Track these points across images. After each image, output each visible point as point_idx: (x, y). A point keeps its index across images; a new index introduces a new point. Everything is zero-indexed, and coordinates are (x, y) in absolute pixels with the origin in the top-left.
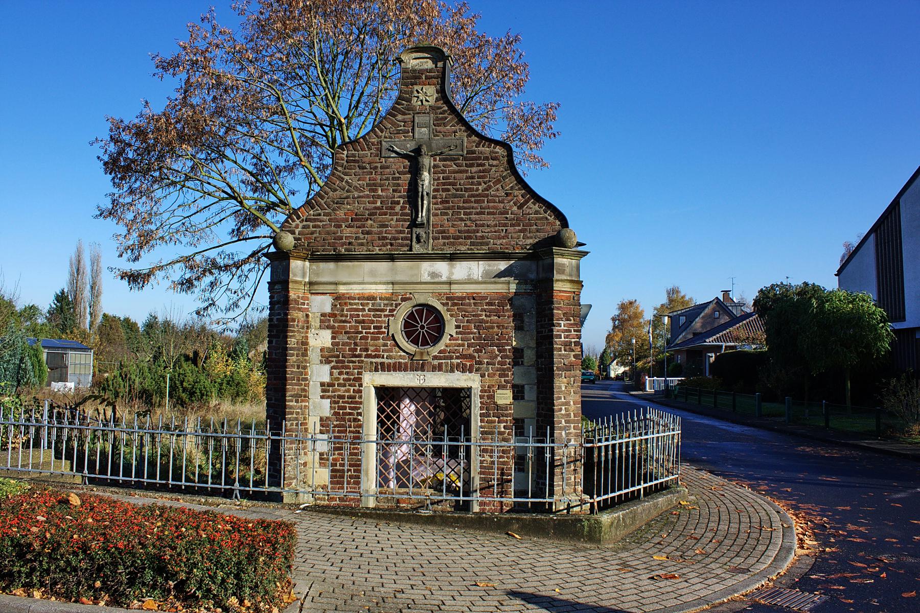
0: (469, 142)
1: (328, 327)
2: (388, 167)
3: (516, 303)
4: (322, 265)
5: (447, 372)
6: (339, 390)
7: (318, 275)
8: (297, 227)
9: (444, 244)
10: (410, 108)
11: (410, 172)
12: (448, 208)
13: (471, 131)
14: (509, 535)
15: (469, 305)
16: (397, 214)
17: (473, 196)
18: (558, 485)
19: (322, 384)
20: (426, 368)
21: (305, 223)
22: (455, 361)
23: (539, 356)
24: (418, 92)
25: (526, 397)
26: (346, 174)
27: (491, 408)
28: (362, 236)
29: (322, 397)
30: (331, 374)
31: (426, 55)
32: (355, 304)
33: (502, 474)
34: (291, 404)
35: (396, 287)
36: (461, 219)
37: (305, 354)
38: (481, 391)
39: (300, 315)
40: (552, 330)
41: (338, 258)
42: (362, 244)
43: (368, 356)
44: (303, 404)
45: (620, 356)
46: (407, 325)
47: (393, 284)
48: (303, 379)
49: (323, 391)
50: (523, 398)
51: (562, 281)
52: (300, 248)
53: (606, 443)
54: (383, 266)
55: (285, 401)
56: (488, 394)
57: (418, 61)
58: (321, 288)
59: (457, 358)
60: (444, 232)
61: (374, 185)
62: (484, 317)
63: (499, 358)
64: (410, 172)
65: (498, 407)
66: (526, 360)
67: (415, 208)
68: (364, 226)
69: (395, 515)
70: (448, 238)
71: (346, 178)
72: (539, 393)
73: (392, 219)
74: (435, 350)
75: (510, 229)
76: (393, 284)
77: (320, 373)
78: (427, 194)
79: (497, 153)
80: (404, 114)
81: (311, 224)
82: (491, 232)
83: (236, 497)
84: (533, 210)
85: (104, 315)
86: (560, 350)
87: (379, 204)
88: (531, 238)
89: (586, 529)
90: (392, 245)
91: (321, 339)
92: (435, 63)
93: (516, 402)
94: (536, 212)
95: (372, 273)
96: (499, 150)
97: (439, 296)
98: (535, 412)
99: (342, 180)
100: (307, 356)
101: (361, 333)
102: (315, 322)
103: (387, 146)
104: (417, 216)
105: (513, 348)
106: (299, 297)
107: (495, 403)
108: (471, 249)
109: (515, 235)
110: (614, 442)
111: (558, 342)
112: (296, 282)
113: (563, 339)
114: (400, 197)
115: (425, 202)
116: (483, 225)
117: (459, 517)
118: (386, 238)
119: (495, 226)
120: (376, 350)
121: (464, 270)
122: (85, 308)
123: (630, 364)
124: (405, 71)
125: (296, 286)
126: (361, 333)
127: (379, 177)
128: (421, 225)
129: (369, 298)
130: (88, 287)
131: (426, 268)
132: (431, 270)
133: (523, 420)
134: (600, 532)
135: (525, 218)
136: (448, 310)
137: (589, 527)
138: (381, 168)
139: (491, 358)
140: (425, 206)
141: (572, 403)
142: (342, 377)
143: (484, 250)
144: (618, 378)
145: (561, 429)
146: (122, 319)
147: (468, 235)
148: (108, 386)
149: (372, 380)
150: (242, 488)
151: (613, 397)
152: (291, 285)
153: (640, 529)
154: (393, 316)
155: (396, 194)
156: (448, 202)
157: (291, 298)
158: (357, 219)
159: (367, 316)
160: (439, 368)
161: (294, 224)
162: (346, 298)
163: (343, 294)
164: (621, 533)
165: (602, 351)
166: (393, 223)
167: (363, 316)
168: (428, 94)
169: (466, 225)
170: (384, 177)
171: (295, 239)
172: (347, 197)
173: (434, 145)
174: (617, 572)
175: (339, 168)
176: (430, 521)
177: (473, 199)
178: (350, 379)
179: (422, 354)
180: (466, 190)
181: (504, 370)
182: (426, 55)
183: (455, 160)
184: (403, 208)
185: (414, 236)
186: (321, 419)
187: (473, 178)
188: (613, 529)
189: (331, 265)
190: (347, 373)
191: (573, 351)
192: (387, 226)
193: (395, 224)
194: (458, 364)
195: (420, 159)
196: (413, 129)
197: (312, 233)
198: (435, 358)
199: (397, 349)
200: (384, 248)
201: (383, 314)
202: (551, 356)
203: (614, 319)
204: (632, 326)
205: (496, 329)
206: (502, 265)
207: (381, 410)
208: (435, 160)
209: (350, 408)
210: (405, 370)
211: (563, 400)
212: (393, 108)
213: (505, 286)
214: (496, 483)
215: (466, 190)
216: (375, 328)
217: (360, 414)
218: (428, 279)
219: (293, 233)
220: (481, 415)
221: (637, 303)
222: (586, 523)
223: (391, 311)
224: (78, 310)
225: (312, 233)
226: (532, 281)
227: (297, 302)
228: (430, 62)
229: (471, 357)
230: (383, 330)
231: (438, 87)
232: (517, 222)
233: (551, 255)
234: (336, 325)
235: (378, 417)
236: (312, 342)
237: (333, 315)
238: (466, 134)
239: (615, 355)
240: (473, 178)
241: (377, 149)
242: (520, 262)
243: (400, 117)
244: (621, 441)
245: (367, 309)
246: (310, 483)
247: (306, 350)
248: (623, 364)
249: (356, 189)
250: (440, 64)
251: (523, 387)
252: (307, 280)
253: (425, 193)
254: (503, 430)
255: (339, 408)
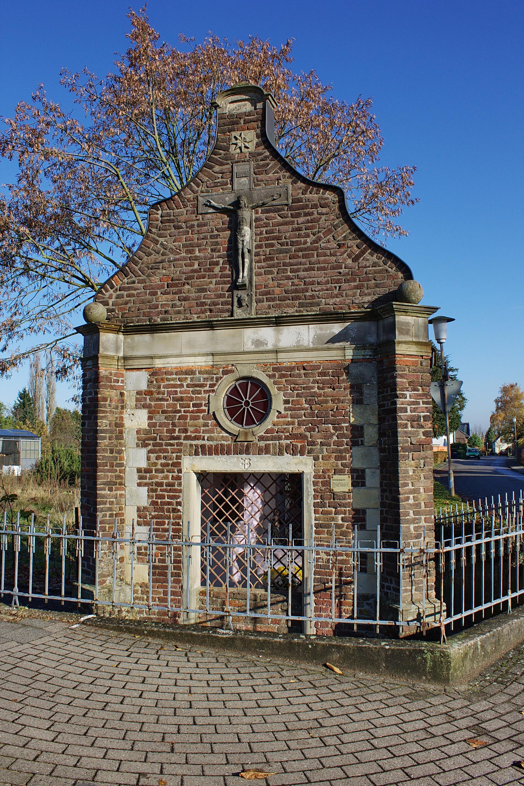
0: (294, 189)
1: (144, 407)
2: (205, 225)
3: (353, 371)
4: (138, 338)
5: (275, 454)
6: (157, 477)
7: (132, 348)
8: (110, 297)
9: (269, 307)
10: (228, 158)
11: (229, 228)
12: (273, 266)
13: (297, 176)
14: (327, 667)
15: (299, 376)
16: (216, 276)
17: (301, 250)
18: (406, 591)
19: (139, 470)
20: (251, 450)
21: (118, 292)
22: (284, 442)
23: (381, 434)
24: (236, 138)
25: (367, 484)
26: (160, 236)
27: (326, 496)
28: (178, 303)
29: (139, 485)
30: (148, 459)
31: (244, 97)
32: (173, 380)
33: (341, 575)
34: (103, 492)
35: (217, 358)
36: (288, 278)
37: (120, 436)
38: (315, 477)
39: (114, 394)
40: (395, 403)
41: (153, 329)
42: (179, 312)
43: (187, 438)
44: (119, 492)
45: (504, 434)
46: (230, 401)
47: (213, 355)
48: (117, 465)
49: (140, 478)
50: (363, 485)
51: (406, 343)
52: (114, 320)
53: (458, 546)
54: (202, 336)
55: (96, 489)
56: (323, 480)
57: (235, 105)
58: (136, 363)
59: (287, 438)
60: (268, 293)
61: (191, 245)
62: (316, 390)
63: (335, 438)
64: (229, 228)
65: (334, 495)
66: (366, 438)
67: (235, 268)
68: (180, 292)
69: (187, 635)
70: (273, 300)
71: (161, 240)
72: (383, 478)
73: (211, 283)
74: (260, 430)
75: (344, 286)
76: (213, 355)
77: (136, 458)
78: (249, 251)
79: (327, 199)
80: (222, 164)
81: (125, 293)
82: (323, 290)
83: (15, 604)
84: (370, 263)
85: (57, 408)
86: (406, 426)
87: (196, 266)
88: (369, 294)
89: (429, 664)
90: (211, 311)
91: (137, 420)
92: (254, 105)
93: (356, 489)
94: (375, 265)
95: (191, 344)
96: (330, 196)
97: (265, 366)
98: (379, 501)
99: (156, 242)
100: (122, 438)
101: (180, 411)
102: (130, 400)
103: (205, 201)
104: (238, 277)
105: (351, 425)
106: (111, 374)
107: (331, 491)
108: (300, 311)
109: (350, 293)
110: (469, 544)
111: (402, 417)
112: (107, 357)
113: (409, 413)
114: (219, 257)
115: (247, 260)
116: (312, 283)
117: (265, 641)
118: (204, 304)
119: (327, 282)
120: (196, 431)
121: (293, 336)
122: (43, 403)
123: (513, 441)
124: (222, 117)
125: (107, 361)
126: (180, 411)
127: (196, 236)
128: (243, 287)
129: (186, 373)
130: (45, 386)
131: (249, 336)
132: (255, 337)
133: (364, 511)
134: (448, 669)
135: (362, 272)
136: (275, 383)
137: (434, 661)
138: (198, 226)
139: (325, 437)
140: (247, 265)
141: (422, 490)
142: (160, 462)
143: (315, 310)
144: (501, 453)
145: (408, 522)
146: (72, 411)
147: (295, 295)
148: (42, 469)
149: (192, 465)
150: (21, 594)
151: (495, 472)
152: (100, 361)
153: (504, 658)
154: (213, 391)
155: (215, 254)
156: (272, 259)
157: (101, 375)
158: (174, 284)
159: (185, 392)
160: (266, 450)
161: (107, 294)
162: (163, 373)
163: (160, 369)
164: (479, 665)
165: (487, 430)
166: (212, 286)
167: (181, 392)
168: (249, 138)
169: (293, 284)
170: (201, 236)
171: (108, 311)
172: (162, 261)
173: (255, 196)
174: (463, 747)
175: (154, 230)
176: (228, 644)
177: (300, 254)
178: (167, 465)
179: (246, 434)
180: (293, 244)
181: (340, 451)
182: (244, 97)
183: (279, 210)
184: (222, 269)
185: (236, 300)
186: (139, 509)
187: (300, 229)
188: (468, 663)
189: (147, 337)
190: (165, 458)
191: (422, 427)
192: (205, 290)
193: (215, 286)
194: (288, 446)
195: (240, 212)
196: (232, 181)
197: (126, 303)
198: (261, 438)
199: (219, 429)
200: (203, 315)
201: (202, 389)
202: (395, 434)
203: (497, 401)
204: (514, 406)
205: (330, 404)
206: (336, 328)
207: (205, 498)
208: (257, 213)
209: (169, 497)
210: (228, 453)
211: (410, 486)
212: (210, 159)
213: (340, 353)
214: (333, 585)
215: (293, 244)
216: (194, 405)
217: (179, 504)
218: (252, 348)
219: (106, 304)
220: (316, 505)
221: (518, 386)
222: (429, 656)
223: (212, 386)
224: (37, 405)
225: (126, 303)
226: (372, 345)
227: (109, 380)
228: (248, 104)
229: (302, 437)
230: (203, 408)
231: (258, 131)
232: (352, 276)
233: (392, 312)
234: (153, 403)
235: (203, 506)
236: (127, 423)
237: (149, 393)
238: (290, 180)
239: (499, 433)
240: (300, 229)
241: (193, 205)
242: (357, 324)
243: (217, 168)
244: (478, 542)
245: (185, 384)
246: (128, 580)
247: (121, 432)
248: (507, 441)
249: (172, 251)
250: (259, 105)
251: (363, 471)
252: (121, 354)
253: (246, 250)
254: (340, 522)
255: (158, 497)
